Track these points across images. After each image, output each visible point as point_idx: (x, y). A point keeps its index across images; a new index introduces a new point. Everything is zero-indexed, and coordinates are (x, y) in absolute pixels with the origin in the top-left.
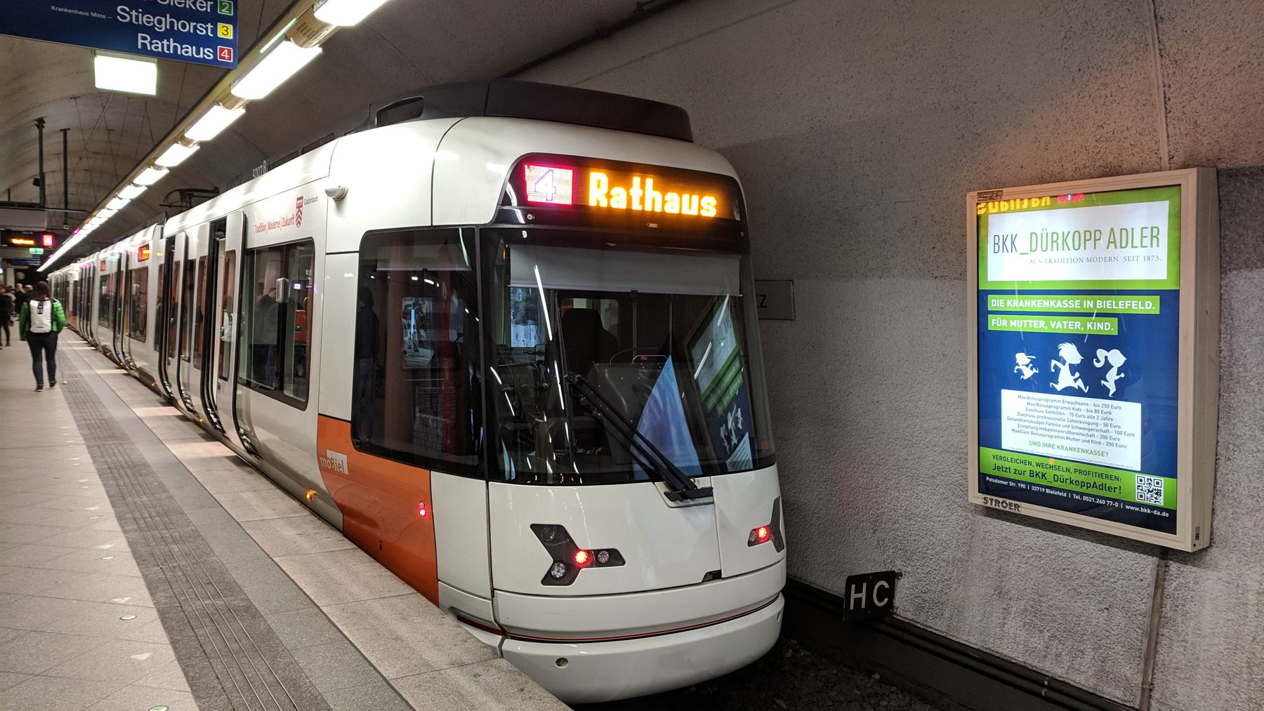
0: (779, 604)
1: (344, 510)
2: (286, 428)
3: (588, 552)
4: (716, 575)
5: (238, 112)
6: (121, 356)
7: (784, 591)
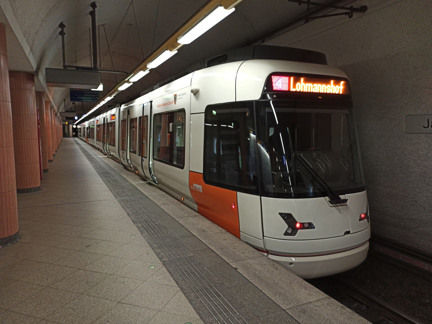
0: (367, 246)
1: (198, 204)
2: (179, 177)
3: (300, 224)
4: (348, 233)
5: (147, 72)
6: (106, 151)
7: (370, 240)
